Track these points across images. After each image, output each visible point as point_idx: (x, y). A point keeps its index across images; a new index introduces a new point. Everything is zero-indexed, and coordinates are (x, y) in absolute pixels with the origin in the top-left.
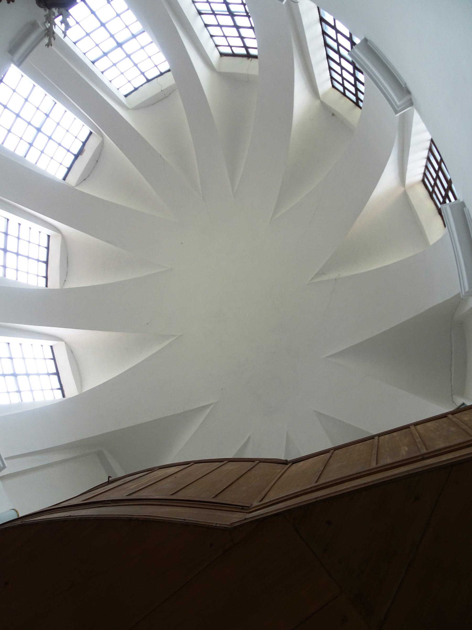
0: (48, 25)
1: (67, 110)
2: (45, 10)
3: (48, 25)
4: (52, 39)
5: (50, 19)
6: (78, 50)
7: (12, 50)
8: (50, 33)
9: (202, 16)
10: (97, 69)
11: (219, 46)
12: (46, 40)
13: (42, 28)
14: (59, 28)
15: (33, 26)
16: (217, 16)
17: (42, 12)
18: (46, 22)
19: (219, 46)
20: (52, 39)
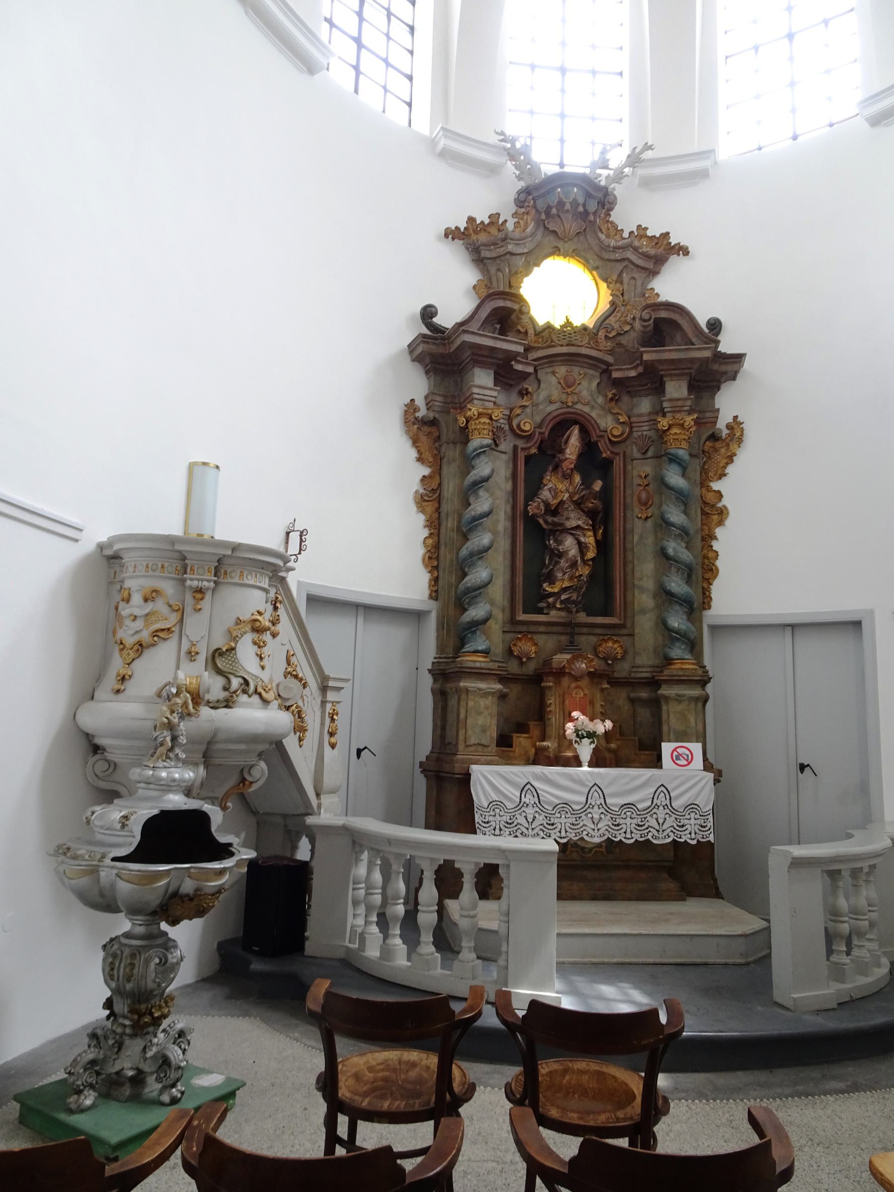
0: (627, 170)
1: (626, 74)
2: (614, 189)
3: (627, 170)
4: (637, 150)
5: (619, 176)
6: (623, 108)
7: (703, 175)
8: (634, 160)
9: (411, 24)
10: (623, 62)
11: (408, 50)
12: (648, 155)
13: (640, 172)
14: (617, 158)
15: (647, 183)
16: (386, 6)
17: (619, 191)
18: (627, 176)
19: (408, 50)
20: (637, 150)
